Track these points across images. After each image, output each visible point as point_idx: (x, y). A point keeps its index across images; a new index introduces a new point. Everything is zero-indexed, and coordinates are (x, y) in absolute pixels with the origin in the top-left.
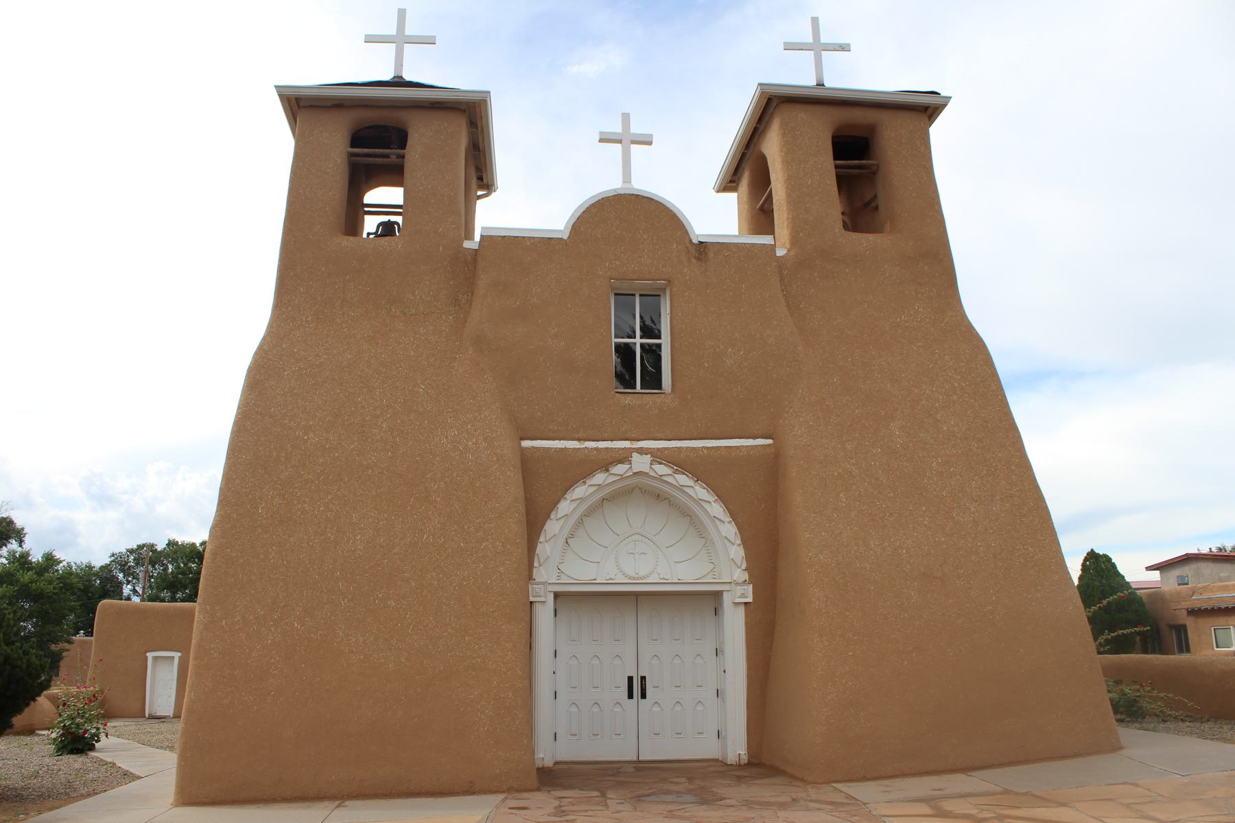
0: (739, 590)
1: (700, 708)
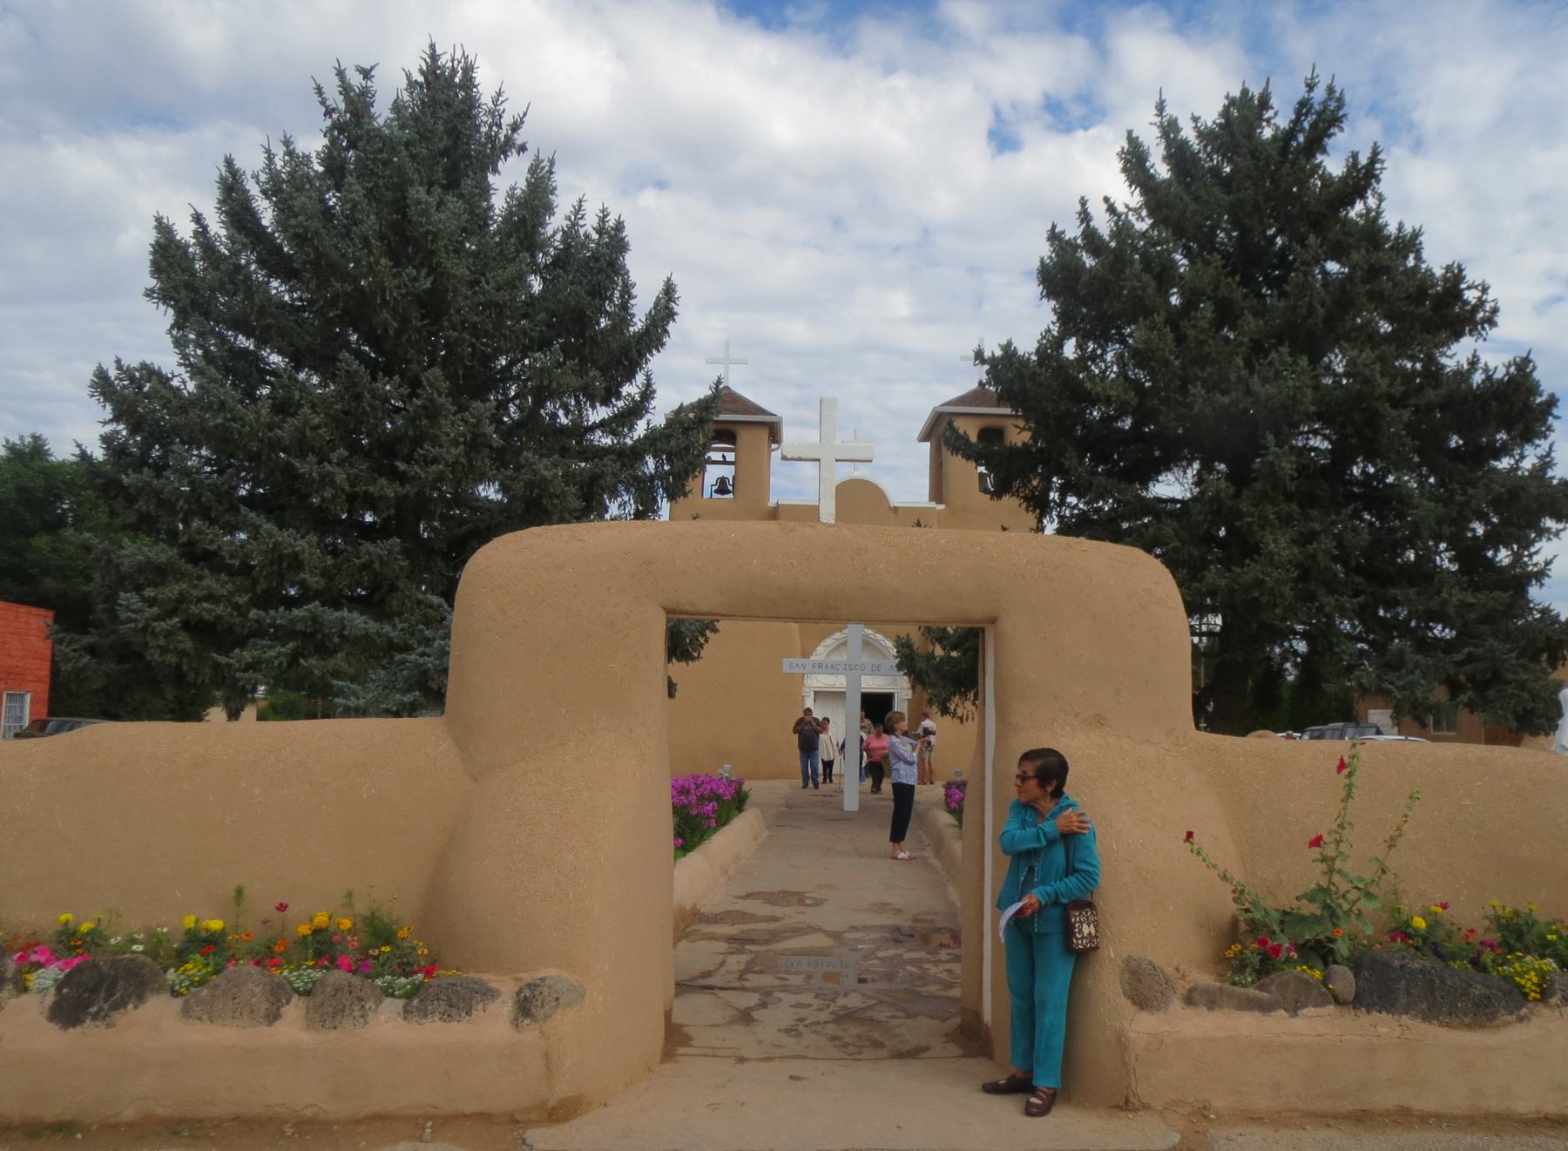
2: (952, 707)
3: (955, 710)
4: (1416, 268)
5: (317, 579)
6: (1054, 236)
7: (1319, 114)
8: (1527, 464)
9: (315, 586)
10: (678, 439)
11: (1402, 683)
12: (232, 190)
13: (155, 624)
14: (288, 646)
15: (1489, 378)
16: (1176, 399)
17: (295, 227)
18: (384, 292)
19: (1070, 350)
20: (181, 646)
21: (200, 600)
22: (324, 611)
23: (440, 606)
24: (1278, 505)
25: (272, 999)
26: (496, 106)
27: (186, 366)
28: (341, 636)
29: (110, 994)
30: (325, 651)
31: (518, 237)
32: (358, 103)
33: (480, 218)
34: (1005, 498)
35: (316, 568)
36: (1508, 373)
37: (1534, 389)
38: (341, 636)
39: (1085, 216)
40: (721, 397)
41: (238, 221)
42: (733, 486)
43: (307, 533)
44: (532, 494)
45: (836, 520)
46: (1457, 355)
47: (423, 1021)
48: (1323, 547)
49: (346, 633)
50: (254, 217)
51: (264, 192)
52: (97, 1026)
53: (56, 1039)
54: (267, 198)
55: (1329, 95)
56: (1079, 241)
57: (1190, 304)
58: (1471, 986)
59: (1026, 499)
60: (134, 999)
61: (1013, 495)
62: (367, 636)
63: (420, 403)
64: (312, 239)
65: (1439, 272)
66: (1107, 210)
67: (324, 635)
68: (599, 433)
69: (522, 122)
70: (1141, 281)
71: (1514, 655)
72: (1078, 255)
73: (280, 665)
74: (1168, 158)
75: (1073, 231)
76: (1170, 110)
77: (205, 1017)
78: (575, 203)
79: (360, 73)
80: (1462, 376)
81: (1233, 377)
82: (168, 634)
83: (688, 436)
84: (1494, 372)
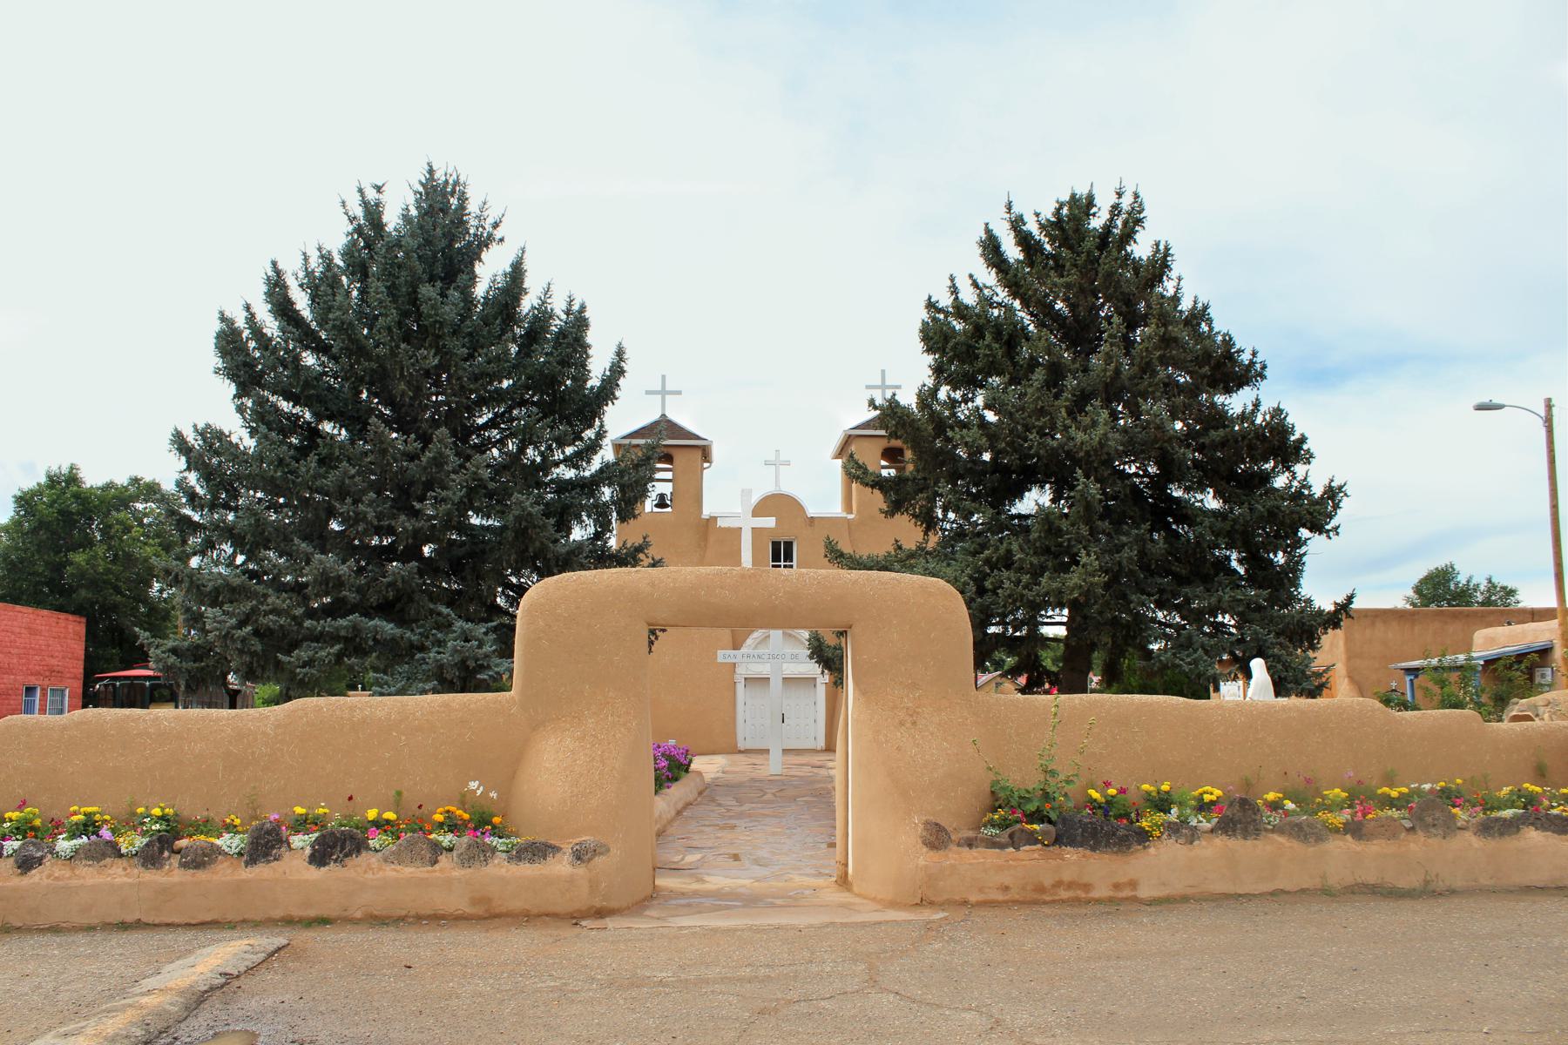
6: (931, 305)
7: (1129, 214)
10: (630, 474)
11: (1189, 660)
12: (277, 292)
13: (234, 632)
17: (334, 320)
18: (402, 369)
19: (943, 393)
20: (253, 649)
23: (449, 615)
28: (375, 639)
30: (361, 652)
32: (373, 213)
33: (468, 300)
34: (897, 516)
38: (375, 639)
39: (954, 290)
40: (665, 427)
41: (282, 310)
42: (671, 500)
45: (753, 565)
46: (1236, 403)
49: (378, 637)
50: (290, 303)
51: (301, 286)
53: (315, 873)
59: (914, 516)
62: (393, 639)
63: (431, 455)
64: (347, 330)
67: (361, 639)
68: (562, 466)
70: (991, 350)
73: (330, 662)
74: (1018, 244)
75: (945, 301)
76: (1016, 209)
78: (545, 286)
82: (244, 640)
83: (638, 471)
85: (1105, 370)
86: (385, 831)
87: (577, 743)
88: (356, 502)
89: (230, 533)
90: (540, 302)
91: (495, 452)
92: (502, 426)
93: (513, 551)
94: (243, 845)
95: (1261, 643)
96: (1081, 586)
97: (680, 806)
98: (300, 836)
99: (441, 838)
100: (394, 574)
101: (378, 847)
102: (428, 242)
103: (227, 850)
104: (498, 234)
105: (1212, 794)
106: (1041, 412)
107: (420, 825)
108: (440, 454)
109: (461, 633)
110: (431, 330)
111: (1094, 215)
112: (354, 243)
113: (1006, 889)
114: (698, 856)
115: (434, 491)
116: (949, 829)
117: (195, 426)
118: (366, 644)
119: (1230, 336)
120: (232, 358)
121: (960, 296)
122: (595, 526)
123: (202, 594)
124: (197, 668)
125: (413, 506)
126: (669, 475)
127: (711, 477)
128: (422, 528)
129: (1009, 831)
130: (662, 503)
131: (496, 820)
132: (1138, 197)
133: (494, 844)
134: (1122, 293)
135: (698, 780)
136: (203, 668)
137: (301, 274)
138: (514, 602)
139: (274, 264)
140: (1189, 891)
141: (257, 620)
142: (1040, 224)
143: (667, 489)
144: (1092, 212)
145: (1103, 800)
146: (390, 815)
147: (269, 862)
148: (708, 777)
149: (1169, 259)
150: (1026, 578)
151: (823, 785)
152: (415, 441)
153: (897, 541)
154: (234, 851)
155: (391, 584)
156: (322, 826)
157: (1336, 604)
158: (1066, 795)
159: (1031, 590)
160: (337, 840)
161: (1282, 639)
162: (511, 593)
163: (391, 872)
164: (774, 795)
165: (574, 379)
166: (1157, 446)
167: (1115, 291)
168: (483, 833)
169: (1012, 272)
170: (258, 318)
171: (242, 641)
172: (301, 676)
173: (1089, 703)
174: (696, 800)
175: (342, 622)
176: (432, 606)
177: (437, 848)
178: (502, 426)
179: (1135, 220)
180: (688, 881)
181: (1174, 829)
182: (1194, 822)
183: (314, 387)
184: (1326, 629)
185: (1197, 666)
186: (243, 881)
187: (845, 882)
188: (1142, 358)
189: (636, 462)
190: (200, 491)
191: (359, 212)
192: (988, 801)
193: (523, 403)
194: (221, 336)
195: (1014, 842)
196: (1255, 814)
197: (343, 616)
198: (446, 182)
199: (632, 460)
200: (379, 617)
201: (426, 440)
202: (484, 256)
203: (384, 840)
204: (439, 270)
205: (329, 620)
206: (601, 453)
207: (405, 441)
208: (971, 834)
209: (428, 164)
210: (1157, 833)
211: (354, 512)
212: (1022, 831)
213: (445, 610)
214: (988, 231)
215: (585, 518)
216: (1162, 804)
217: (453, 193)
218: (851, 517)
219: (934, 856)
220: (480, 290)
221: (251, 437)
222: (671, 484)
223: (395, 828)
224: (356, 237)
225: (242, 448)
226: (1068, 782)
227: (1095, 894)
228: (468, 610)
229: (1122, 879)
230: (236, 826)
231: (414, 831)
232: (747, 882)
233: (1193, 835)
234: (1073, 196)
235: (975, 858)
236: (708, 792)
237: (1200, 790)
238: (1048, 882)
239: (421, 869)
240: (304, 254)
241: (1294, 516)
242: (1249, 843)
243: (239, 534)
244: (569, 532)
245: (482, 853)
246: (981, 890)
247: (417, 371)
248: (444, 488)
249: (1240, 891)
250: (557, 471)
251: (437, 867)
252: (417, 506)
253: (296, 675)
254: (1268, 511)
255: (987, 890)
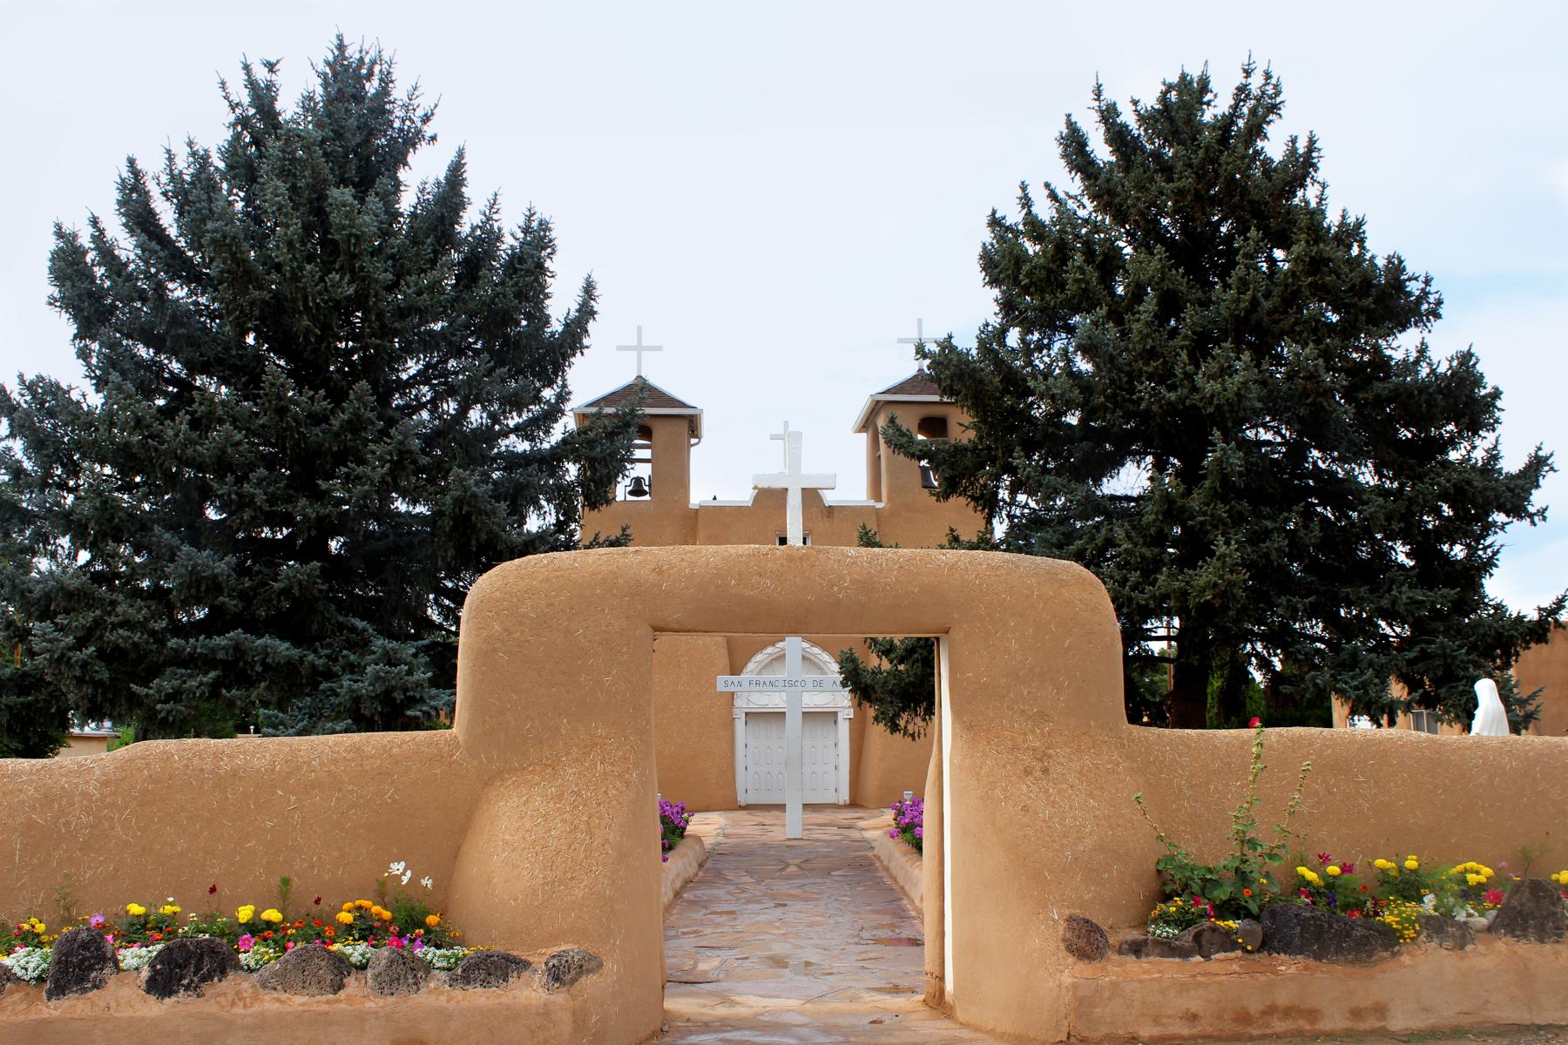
0: (846, 711)
1: (826, 775)
2: (902, 723)
3: (906, 727)
4: (1361, 255)
5: (235, 602)
6: (995, 222)
7: (1258, 99)
8: (1479, 455)
9: (234, 609)
13: (71, 654)
14: (210, 675)
15: (1433, 371)
16: (1123, 396)
17: (213, 232)
19: (1013, 338)
20: (98, 677)
21: (114, 627)
22: (246, 639)
23: (364, 630)
24: (1229, 503)
25: (335, 971)
26: (410, 100)
27: (92, 378)
28: (264, 663)
29: (198, 969)
30: (247, 681)
31: (435, 236)
32: (263, 98)
34: (953, 499)
35: (234, 591)
36: (1451, 368)
37: (1478, 381)
39: (1026, 202)
42: (650, 486)
43: (226, 554)
44: (461, 511)
46: (1402, 345)
47: (467, 987)
48: (1276, 545)
49: (269, 660)
50: (152, 214)
51: (165, 194)
52: (189, 996)
54: (168, 199)
55: (1266, 80)
56: (1021, 227)
57: (1137, 294)
58: (1353, 929)
59: (973, 498)
60: (218, 972)
61: (960, 495)
63: (346, 417)
65: (1381, 262)
66: (1049, 196)
67: (246, 662)
68: (513, 437)
69: (433, 114)
71: (1463, 651)
72: (1021, 241)
74: (1109, 141)
75: (1014, 216)
76: (1108, 96)
77: (279, 987)
78: (491, 197)
79: (265, 65)
80: (1409, 367)
81: (1178, 371)
82: (84, 665)
83: (612, 441)
84: (1438, 366)
85: (1238, 301)
86: (265, 939)
87: (551, 805)
88: (239, 481)
89: (70, 523)
90: (484, 219)
91: (425, 415)
92: (434, 382)
93: (451, 544)
94: (45, 966)
95: (1449, 661)
96: (1215, 585)
97: (678, 885)
98: (135, 950)
99: (348, 950)
100: (288, 577)
101: (252, 964)
102: (338, 136)
103: (20, 973)
104: (428, 130)
105: (1478, 873)
106: (1150, 355)
107: (318, 929)
108: (357, 415)
109: (382, 655)
110: (343, 247)
111: (1208, 104)
112: (237, 137)
113: (1193, 1018)
114: (716, 962)
115: (347, 466)
116: (1104, 928)
117: (21, 376)
118: (252, 669)
119: (1399, 258)
120: (73, 285)
121: (1034, 210)
122: (557, 513)
123: (28, 603)
124: (22, 704)
125: (318, 485)
126: (646, 454)
127: (701, 458)
128: (328, 516)
129: (1193, 930)
130: (637, 490)
131: (432, 919)
132: (1270, 77)
133: (429, 957)
134: (1251, 202)
135: (697, 848)
136: (30, 704)
137: (164, 179)
138: (452, 615)
139: (131, 162)
140: (1465, 1021)
141: (101, 637)
142: (1139, 115)
143: (643, 471)
144: (1205, 99)
145: (1322, 883)
146: (273, 915)
147: (84, 991)
148: (708, 842)
149: (1314, 154)
150: (1134, 576)
151: (861, 853)
152: (325, 399)
153: (952, 530)
154: (32, 974)
155: (285, 592)
156: (169, 933)
157: (1540, 609)
158: (1267, 875)
159: (1142, 592)
160: (190, 955)
161: (1473, 657)
162: (447, 602)
163: (271, 1003)
164: (798, 866)
165: (529, 317)
166: (1309, 400)
167: (1242, 199)
168: (412, 941)
169: (1103, 176)
170: (109, 235)
171: (81, 667)
172: (163, 714)
173: (1291, 740)
174: (696, 875)
175: (218, 640)
176: (341, 619)
177: (342, 967)
178: (434, 382)
179: (1265, 108)
180: (708, 1001)
181: (1438, 926)
182: (1461, 917)
183: (183, 325)
184: (1527, 643)
185: (1366, 692)
186: (47, 1022)
187: (939, 1004)
188: (1286, 286)
189: (609, 429)
190: (28, 465)
191: (244, 96)
192: (1155, 886)
193: (459, 353)
194: (57, 256)
195: (1201, 946)
196: (1554, 904)
197: (221, 633)
198: (361, 60)
199: (605, 427)
200: (270, 634)
201: (338, 396)
202: (411, 158)
203: (263, 955)
204: (352, 172)
205: (201, 638)
206: (561, 422)
207: (312, 399)
208: (1135, 935)
209: (338, 37)
210: (1411, 933)
211: (237, 494)
212: (1214, 929)
213: (360, 624)
214: (1071, 125)
215: (544, 503)
216: (1409, 887)
217: (370, 74)
218: (880, 505)
219: (1084, 969)
220: (407, 202)
221: (98, 391)
222: (650, 465)
223: (280, 935)
224: (239, 129)
225: (86, 409)
226: (1272, 856)
227: (1325, 1025)
228: (390, 624)
229: (1365, 1002)
230: (38, 935)
231: (308, 940)
232: (794, 1003)
233: (1463, 936)
234: (1183, 77)
235: (1146, 972)
236: (714, 864)
237: (1460, 867)
238: (1255, 1007)
239: (318, 998)
240: (168, 151)
241: (1488, 493)
242: (1548, 947)
243: (79, 521)
244: (522, 522)
245: (410, 972)
246: (1156, 1020)
247: (326, 302)
248: (362, 461)
249: (1538, 1021)
250: (507, 442)
251: (342, 994)
252: (323, 485)
253: (157, 712)
254: (1455, 485)
255: (1164, 1021)
